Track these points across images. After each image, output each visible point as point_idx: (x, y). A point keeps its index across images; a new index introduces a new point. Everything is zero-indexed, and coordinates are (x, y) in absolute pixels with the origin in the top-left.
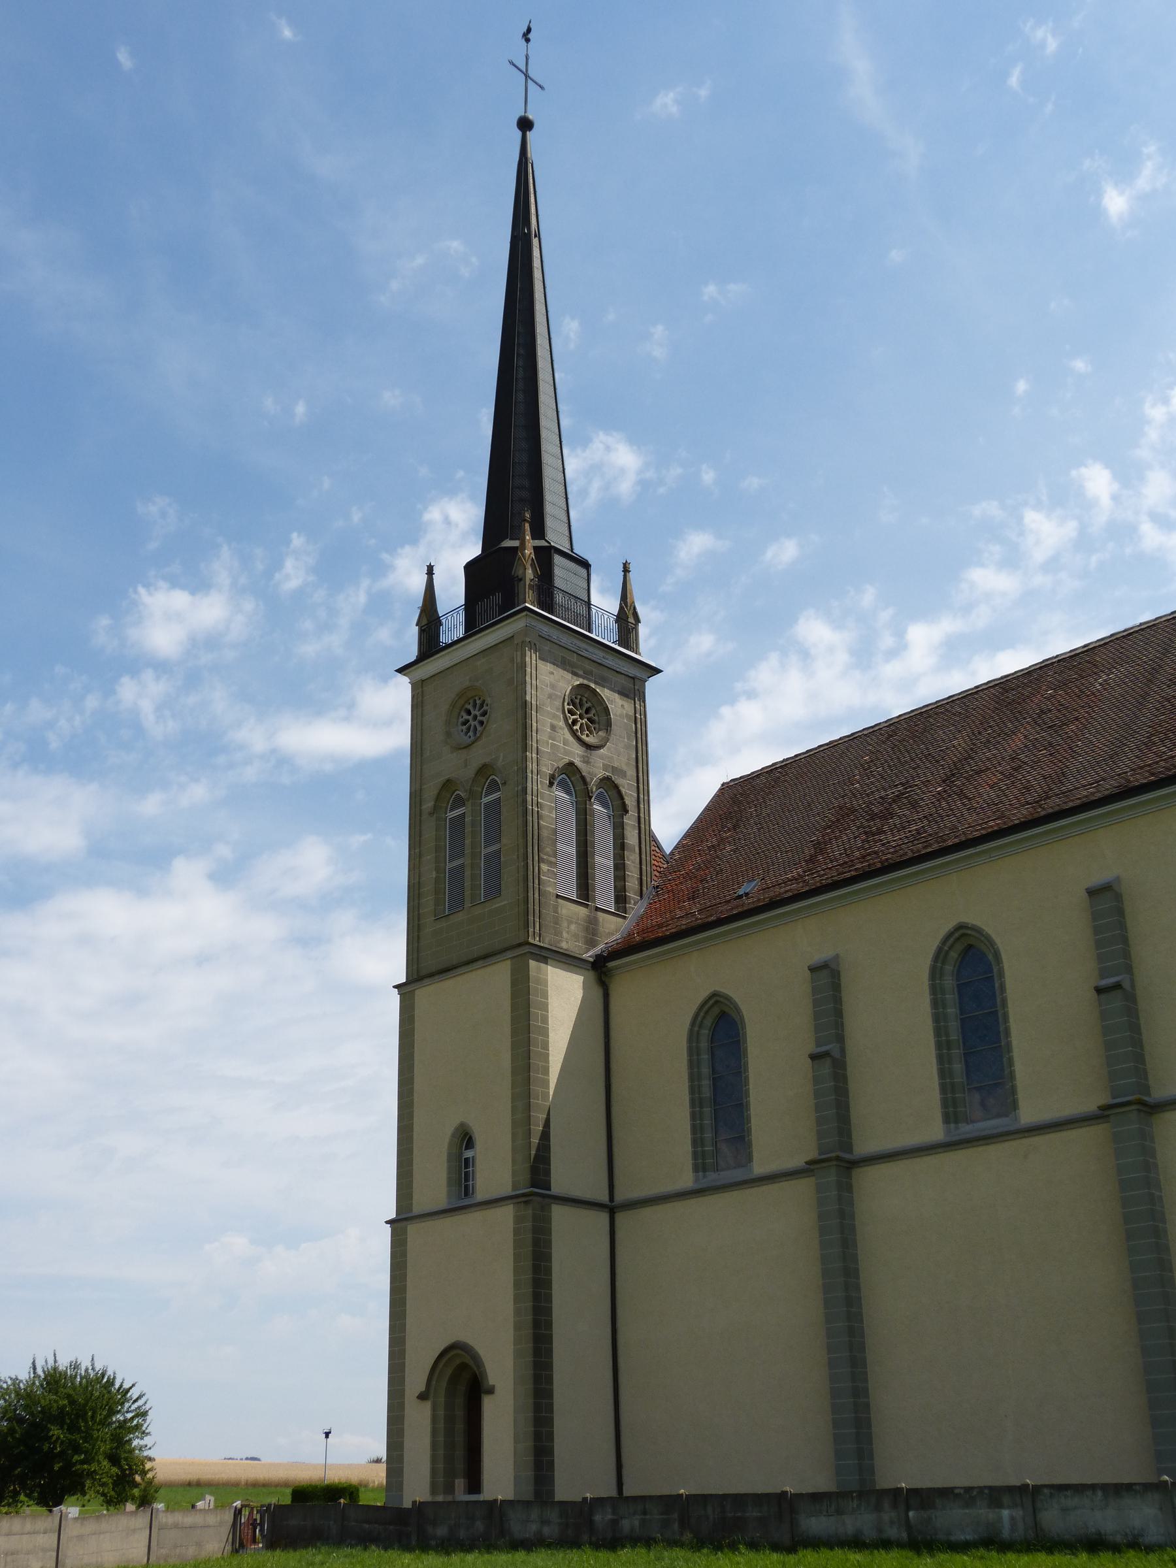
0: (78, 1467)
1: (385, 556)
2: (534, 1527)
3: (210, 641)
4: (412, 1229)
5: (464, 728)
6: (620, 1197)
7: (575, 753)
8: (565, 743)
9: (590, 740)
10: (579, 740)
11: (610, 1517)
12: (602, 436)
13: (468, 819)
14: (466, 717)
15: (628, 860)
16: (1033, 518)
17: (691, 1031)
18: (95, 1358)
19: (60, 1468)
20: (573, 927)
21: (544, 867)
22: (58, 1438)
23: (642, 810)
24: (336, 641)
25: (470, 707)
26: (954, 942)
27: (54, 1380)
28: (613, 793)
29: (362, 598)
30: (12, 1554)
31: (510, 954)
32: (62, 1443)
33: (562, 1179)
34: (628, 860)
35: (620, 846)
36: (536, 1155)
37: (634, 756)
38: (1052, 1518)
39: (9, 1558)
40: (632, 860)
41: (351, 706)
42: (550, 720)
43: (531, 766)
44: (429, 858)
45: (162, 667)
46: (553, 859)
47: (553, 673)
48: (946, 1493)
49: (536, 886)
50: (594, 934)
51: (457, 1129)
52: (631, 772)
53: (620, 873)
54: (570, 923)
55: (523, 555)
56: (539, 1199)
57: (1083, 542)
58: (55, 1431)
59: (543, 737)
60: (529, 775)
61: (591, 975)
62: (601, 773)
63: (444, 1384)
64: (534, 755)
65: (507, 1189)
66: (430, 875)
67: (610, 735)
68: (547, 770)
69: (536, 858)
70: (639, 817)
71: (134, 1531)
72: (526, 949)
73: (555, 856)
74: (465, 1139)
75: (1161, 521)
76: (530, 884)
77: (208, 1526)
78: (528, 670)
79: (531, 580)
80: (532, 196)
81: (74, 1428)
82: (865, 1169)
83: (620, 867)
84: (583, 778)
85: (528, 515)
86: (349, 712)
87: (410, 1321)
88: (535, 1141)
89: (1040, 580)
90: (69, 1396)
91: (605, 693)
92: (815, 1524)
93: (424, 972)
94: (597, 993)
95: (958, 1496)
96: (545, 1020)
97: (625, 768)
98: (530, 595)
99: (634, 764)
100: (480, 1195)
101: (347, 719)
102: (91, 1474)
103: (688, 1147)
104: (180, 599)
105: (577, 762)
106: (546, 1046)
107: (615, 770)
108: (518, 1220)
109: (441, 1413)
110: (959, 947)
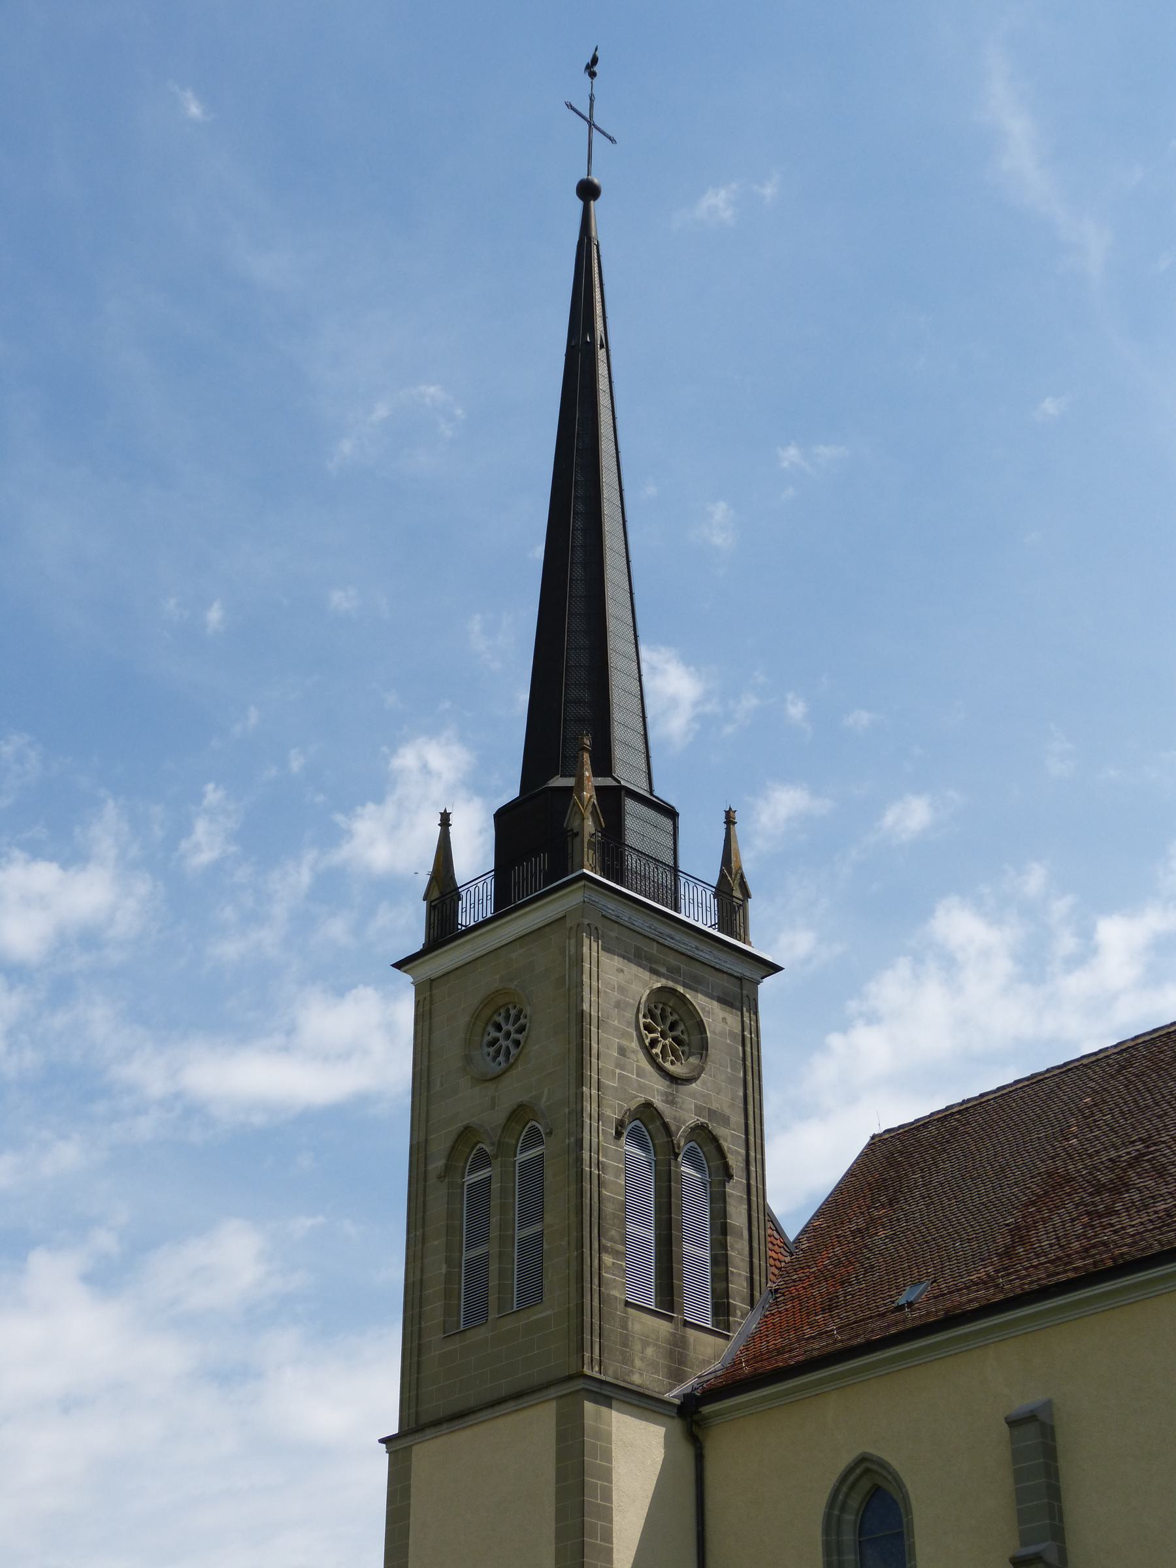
5: (492, 1050)
7: (655, 1089)
8: (640, 1073)
9: (677, 1069)
14: (494, 1034)
20: (650, 1351)
23: (753, 1175)
25: (500, 1019)
28: (710, 1148)
31: (553, 1392)
35: (721, 1228)
37: (741, 1094)
40: (738, 1250)
44: (437, 1243)
46: (620, 1248)
47: (622, 971)
49: (595, 1287)
52: (737, 1118)
54: (645, 1344)
55: (581, 798)
59: (607, 1064)
61: (677, 1425)
62: (692, 1119)
64: (594, 1092)
66: (437, 1269)
67: (705, 1062)
68: (613, 1114)
70: (749, 1186)
72: (579, 1384)
76: (587, 1285)
78: (586, 966)
83: (720, 1260)
85: (587, 742)
91: (699, 1001)
94: (686, 1453)
98: (590, 856)
105: (658, 1102)
106: (608, 1536)
107: (712, 1113)
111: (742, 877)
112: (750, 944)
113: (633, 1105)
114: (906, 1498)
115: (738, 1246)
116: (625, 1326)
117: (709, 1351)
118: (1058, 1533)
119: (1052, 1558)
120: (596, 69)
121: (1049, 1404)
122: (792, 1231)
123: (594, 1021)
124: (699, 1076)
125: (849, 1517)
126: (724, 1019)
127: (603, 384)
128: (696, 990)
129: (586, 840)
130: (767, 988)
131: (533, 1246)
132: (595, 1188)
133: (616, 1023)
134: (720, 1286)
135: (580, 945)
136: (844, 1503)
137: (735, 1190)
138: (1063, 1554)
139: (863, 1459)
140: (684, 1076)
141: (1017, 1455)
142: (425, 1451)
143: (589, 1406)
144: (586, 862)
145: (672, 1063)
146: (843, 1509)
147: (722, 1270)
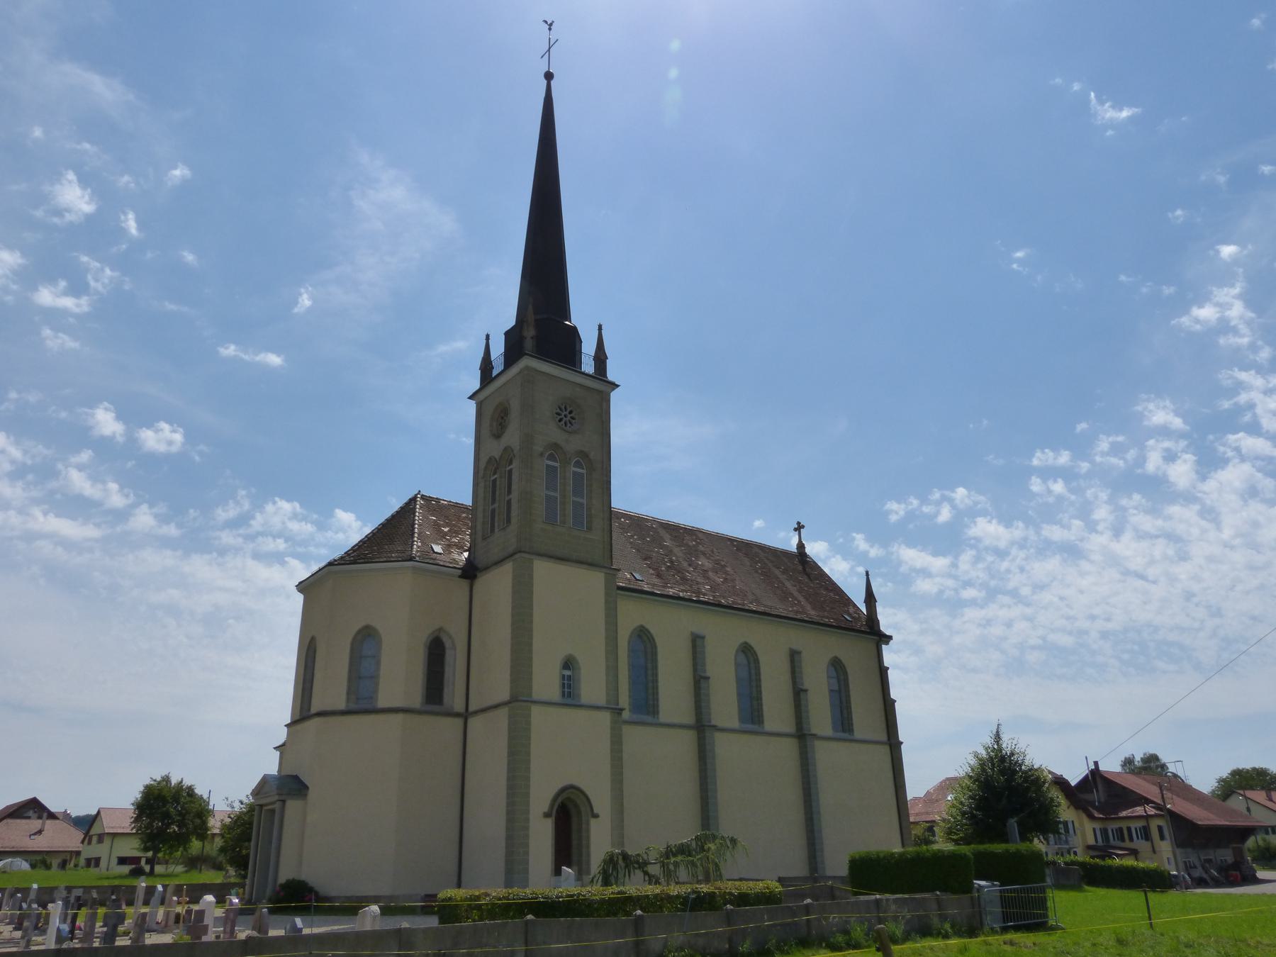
131: (509, 502)
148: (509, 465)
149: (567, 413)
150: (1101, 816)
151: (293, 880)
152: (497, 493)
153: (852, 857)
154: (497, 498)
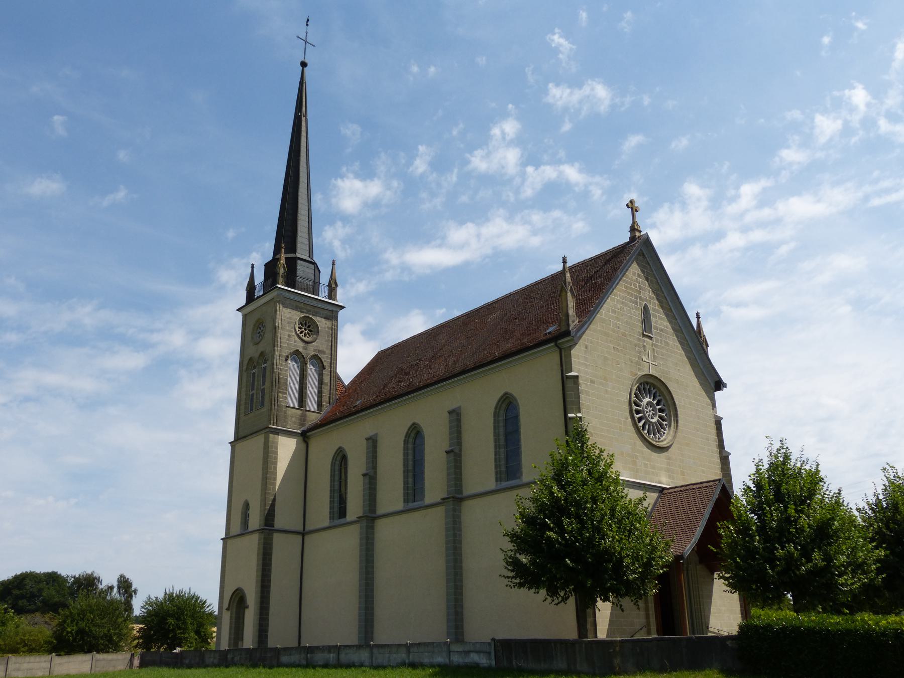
0: (179, 635)
1: (468, 155)
2: (212, 660)
3: (374, 204)
4: (229, 542)
5: (258, 335)
6: (308, 528)
7: (300, 346)
8: (295, 341)
9: (306, 339)
10: (302, 340)
11: (232, 656)
12: (590, 82)
13: (256, 374)
14: (259, 330)
15: (324, 389)
16: (819, 119)
17: (332, 462)
18: (191, 589)
19: (172, 636)
20: (293, 419)
21: (281, 395)
22: (171, 623)
23: (333, 367)
24: (438, 201)
25: (260, 326)
26: (412, 430)
27: (170, 597)
28: (319, 361)
29: (454, 179)
30: (30, 669)
31: (264, 431)
32: (173, 625)
33: (280, 522)
34: (324, 389)
35: (321, 383)
36: (267, 513)
37: (330, 344)
38: (344, 657)
39: (28, 671)
40: (326, 389)
41: (444, 238)
42: (288, 333)
43: (277, 353)
44: (244, 389)
45: (346, 219)
46: (285, 391)
47: (290, 313)
48: (317, 648)
49: (276, 403)
50: (305, 421)
51: (245, 502)
52: (328, 352)
53: (320, 395)
54: (292, 417)
55: (280, 263)
56: (268, 531)
57: (847, 131)
58: (170, 621)
59: (283, 340)
60: (276, 357)
61: (301, 438)
62: (312, 353)
63: (235, 604)
64: (279, 348)
65: (257, 527)
66: (244, 397)
67: (318, 337)
68: (284, 354)
69: (277, 391)
70: (331, 370)
71: (85, 661)
72: (268, 430)
73: (286, 389)
74: (247, 506)
75: (892, 117)
76: (273, 403)
77: (119, 660)
78: (278, 312)
79: (283, 274)
80: (304, 98)
81: (178, 619)
82: (379, 520)
83: (320, 392)
84: (303, 356)
85: (283, 245)
86: (443, 243)
87: (226, 579)
88: (268, 507)
89: (820, 155)
90: (176, 606)
91: (317, 319)
92: (284, 659)
93: (239, 437)
94: (303, 446)
95: (321, 649)
96: (276, 458)
97: (325, 350)
98: (281, 280)
99: (330, 348)
100: (250, 529)
101: (440, 246)
102: (185, 639)
103: (328, 510)
104: (358, 184)
105: (300, 350)
106: (276, 469)
107: (320, 351)
108: (260, 539)
109: (234, 615)
110: (414, 432)
111: (335, 280)
112: (337, 301)
113: (292, 351)
114: (518, 406)
115: (326, 388)
116: (285, 413)
117: (314, 417)
118: (460, 444)
119: (457, 451)
120: (308, 23)
121: (460, 408)
122: (347, 382)
123: (280, 328)
124: (316, 340)
125: (337, 462)
126: (326, 324)
127: (303, 128)
128: (316, 316)
129: (280, 275)
130: (341, 313)
131: (263, 390)
132: (277, 376)
133: (287, 328)
134: (320, 399)
135: (276, 306)
136: (336, 459)
137: (326, 372)
138: (460, 450)
139: (506, 394)
140: (310, 341)
141: (450, 422)
142: (239, 446)
143: (271, 435)
144: (280, 282)
145: (308, 337)
146: (336, 460)
147: (320, 395)
148: (264, 364)
149: (306, 327)
150: (682, 575)
151: (243, 590)
152: (256, 384)
153: (739, 625)
154: (255, 387)
